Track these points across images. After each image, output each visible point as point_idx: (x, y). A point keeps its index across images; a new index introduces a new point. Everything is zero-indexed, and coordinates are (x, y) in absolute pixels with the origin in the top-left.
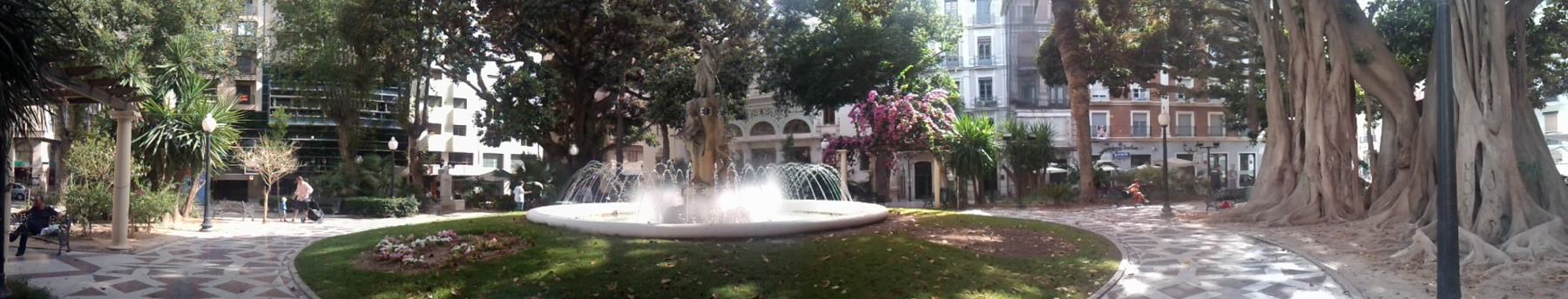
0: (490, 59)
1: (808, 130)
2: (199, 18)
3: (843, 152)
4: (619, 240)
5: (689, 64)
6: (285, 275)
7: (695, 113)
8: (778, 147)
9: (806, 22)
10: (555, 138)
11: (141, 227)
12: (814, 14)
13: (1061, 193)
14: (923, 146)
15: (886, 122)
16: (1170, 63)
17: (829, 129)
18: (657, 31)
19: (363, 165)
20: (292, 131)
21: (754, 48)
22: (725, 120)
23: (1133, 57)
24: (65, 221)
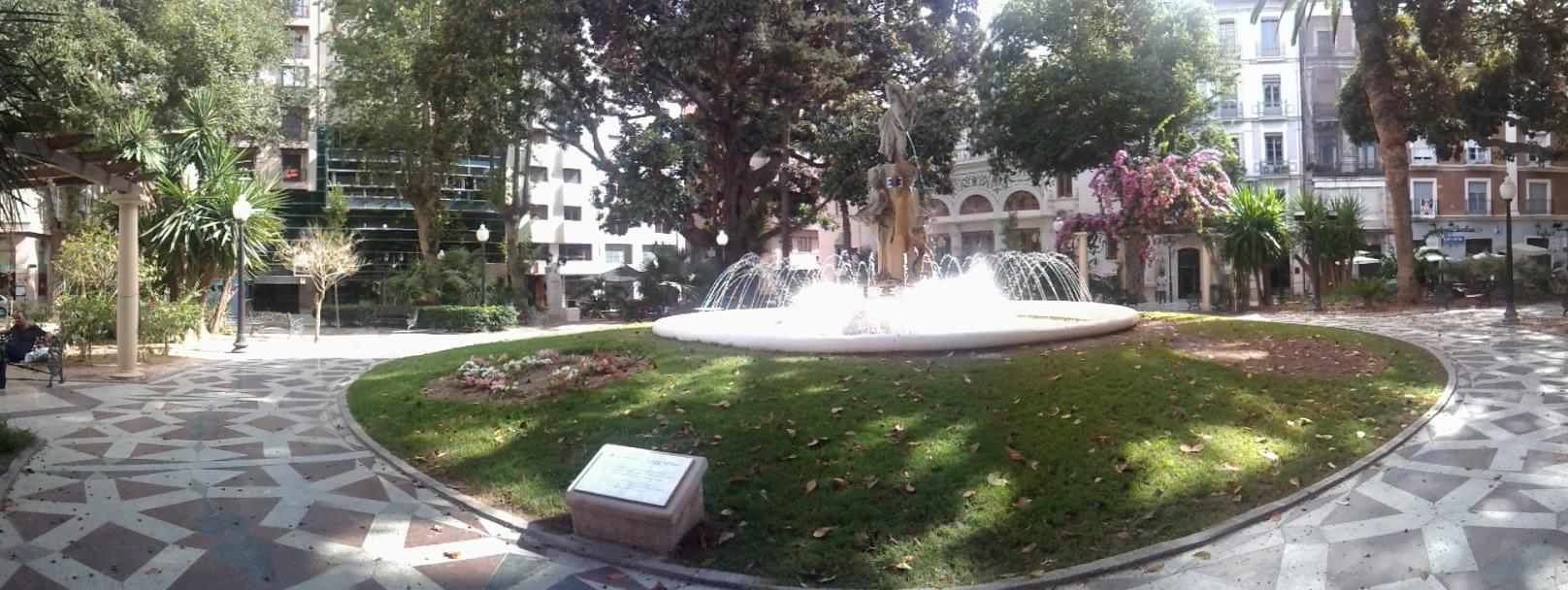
0: (611, 112)
1: (1036, 206)
2: (229, 63)
3: (1083, 235)
4: (764, 358)
5: (874, 117)
6: (333, 413)
7: (880, 185)
8: (997, 229)
9: (1032, 54)
10: (699, 222)
11: (157, 348)
13: (1373, 293)
14: (1187, 228)
16: (1518, 110)
17: (1065, 204)
18: (831, 69)
19: (446, 261)
20: (354, 218)
21: (963, 92)
23: (1468, 102)
24: (56, 342)
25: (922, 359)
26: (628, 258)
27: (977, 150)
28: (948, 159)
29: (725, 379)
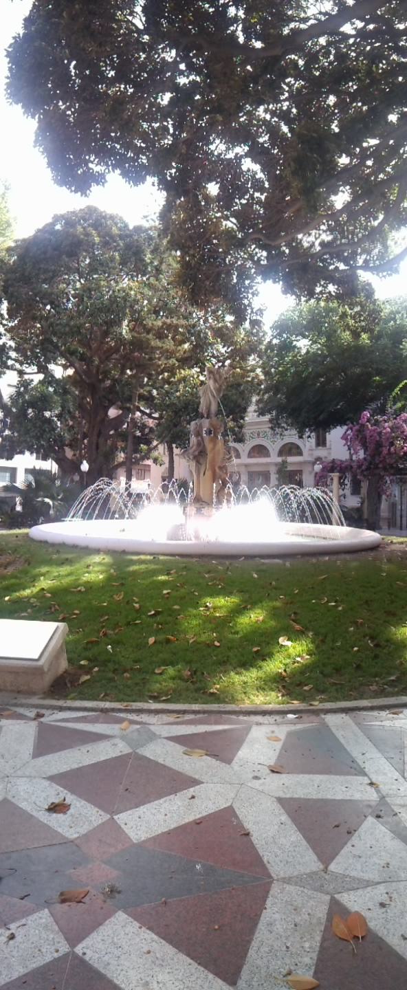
0: (12, 368)
1: (300, 453)
3: (335, 476)
4: (120, 556)
7: (198, 434)
8: (273, 470)
9: (299, 344)
10: (69, 453)
12: (304, 337)
15: (379, 445)
17: (321, 452)
18: (169, 354)
22: (226, 442)
25: (223, 561)
26: (13, 477)
27: (261, 413)
28: (243, 418)
29: (94, 572)
